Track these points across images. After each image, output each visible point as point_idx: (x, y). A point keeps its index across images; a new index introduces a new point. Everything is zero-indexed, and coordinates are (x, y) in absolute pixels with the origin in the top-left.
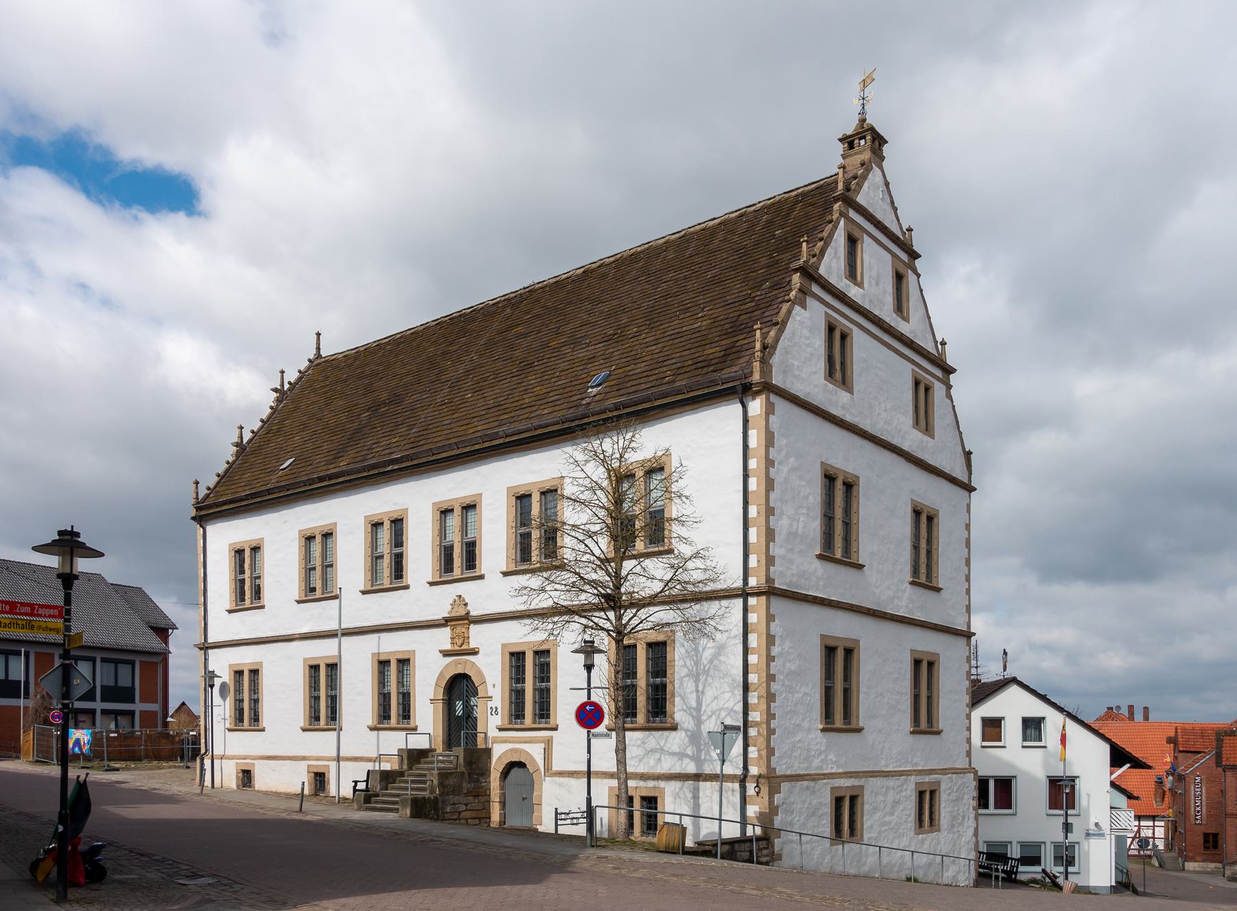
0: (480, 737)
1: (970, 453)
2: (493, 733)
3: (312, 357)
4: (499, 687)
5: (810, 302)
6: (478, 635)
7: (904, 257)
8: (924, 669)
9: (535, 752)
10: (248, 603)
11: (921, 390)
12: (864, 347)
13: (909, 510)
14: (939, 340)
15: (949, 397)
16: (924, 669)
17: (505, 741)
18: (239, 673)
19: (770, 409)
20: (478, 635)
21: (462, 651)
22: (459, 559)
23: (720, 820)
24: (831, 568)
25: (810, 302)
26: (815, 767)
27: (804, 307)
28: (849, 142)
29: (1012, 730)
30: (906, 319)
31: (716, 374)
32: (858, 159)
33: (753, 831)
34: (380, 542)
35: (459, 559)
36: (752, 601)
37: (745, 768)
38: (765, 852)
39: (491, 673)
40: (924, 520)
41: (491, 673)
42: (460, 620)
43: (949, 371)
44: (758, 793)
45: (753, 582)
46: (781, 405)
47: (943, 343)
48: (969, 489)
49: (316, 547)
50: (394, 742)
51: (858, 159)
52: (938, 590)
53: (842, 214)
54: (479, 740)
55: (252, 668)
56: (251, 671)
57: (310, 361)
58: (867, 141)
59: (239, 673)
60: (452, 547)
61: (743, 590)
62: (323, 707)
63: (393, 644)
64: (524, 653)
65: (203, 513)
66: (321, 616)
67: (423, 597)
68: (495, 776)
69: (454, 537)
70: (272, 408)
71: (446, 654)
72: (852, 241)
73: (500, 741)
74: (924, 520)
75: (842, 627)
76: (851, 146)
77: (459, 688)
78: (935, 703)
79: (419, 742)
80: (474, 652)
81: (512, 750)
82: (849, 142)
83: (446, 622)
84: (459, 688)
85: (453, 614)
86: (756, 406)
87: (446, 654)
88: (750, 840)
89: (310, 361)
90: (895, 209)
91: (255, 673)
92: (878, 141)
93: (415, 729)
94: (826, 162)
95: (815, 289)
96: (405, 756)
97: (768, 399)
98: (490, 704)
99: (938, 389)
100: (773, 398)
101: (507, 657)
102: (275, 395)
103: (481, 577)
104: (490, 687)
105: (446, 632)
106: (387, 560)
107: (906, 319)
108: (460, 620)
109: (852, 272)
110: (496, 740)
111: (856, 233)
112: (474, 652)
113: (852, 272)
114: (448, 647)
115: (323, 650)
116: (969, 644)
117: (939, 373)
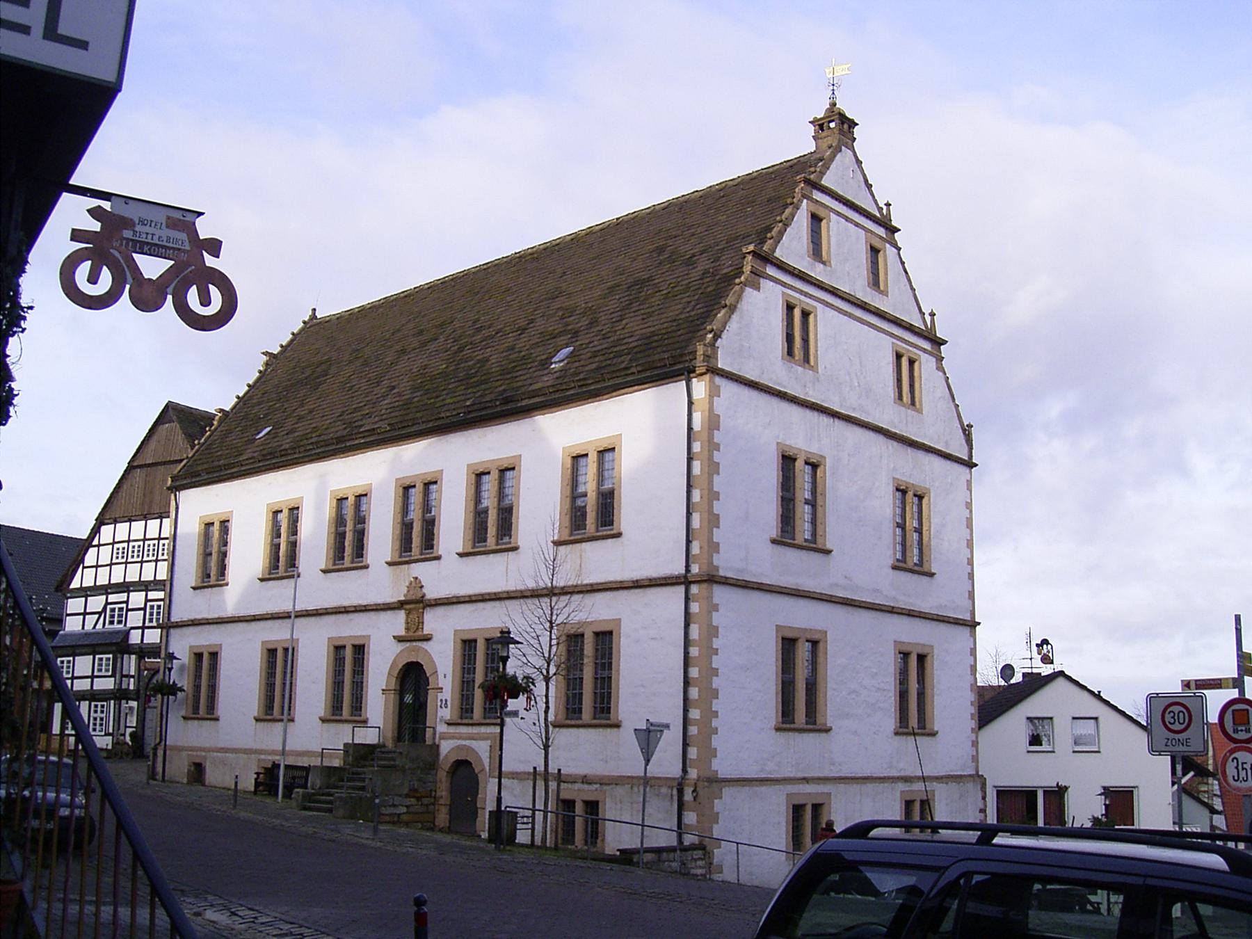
0: (429, 732)
1: (970, 426)
2: (442, 728)
3: (306, 319)
4: (449, 678)
5: (765, 284)
6: (433, 621)
7: (881, 231)
8: (914, 668)
9: (482, 749)
10: (347, 562)
11: (904, 365)
12: (829, 325)
13: (891, 488)
14: (927, 312)
15: (941, 368)
16: (914, 668)
17: (452, 737)
18: (199, 656)
19: (714, 392)
20: (433, 621)
21: (415, 635)
22: (417, 538)
23: (643, 826)
24: (791, 555)
25: (765, 284)
26: (772, 770)
27: (758, 289)
28: (820, 125)
29: (1063, 733)
30: (885, 293)
31: (666, 355)
32: (829, 141)
33: (689, 839)
34: (485, 495)
35: (417, 538)
36: (694, 589)
37: (685, 771)
38: (700, 863)
39: (442, 660)
40: (909, 497)
41: (442, 660)
42: (415, 604)
43: (938, 343)
44: (695, 799)
45: (695, 569)
46: (727, 387)
47: (932, 315)
48: (970, 465)
49: (489, 484)
50: (341, 736)
51: (829, 141)
52: (932, 575)
53: (804, 196)
54: (428, 735)
55: (211, 650)
56: (211, 654)
57: (304, 322)
58: (837, 127)
59: (199, 656)
60: (486, 511)
61: (685, 577)
62: (276, 700)
63: (351, 628)
64: (475, 641)
65: (178, 483)
66: (279, 597)
67: (379, 580)
68: (442, 775)
69: (489, 501)
70: (260, 372)
71: (400, 639)
72: (816, 219)
73: (448, 735)
74: (909, 497)
75: (802, 616)
76: (821, 127)
77: (412, 679)
78: (928, 699)
79: (368, 737)
80: (427, 639)
81: (458, 747)
82: (820, 125)
83: (400, 605)
84: (412, 679)
85: (409, 598)
86: (700, 388)
87: (400, 639)
88: (686, 850)
89: (304, 322)
90: (869, 186)
91: (214, 656)
92: (847, 125)
93: (365, 722)
94: (803, 144)
95: (770, 271)
96: (351, 752)
97: (712, 381)
98: (440, 696)
99: (926, 364)
100: (718, 380)
101: (459, 645)
102: (265, 358)
103: (438, 558)
104: (441, 677)
105: (401, 616)
106: (215, 556)
107: (885, 293)
108: (415, 604)
109: (816, 251)
110: (444, 737)
111: (821, 212)
112: (427, 639)
113: (816, 251)
114: (402, 632)
115: (277, 633)
116: (973, 635)
117: (926, 345)
